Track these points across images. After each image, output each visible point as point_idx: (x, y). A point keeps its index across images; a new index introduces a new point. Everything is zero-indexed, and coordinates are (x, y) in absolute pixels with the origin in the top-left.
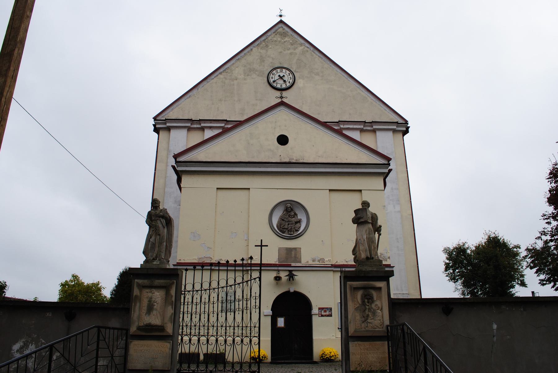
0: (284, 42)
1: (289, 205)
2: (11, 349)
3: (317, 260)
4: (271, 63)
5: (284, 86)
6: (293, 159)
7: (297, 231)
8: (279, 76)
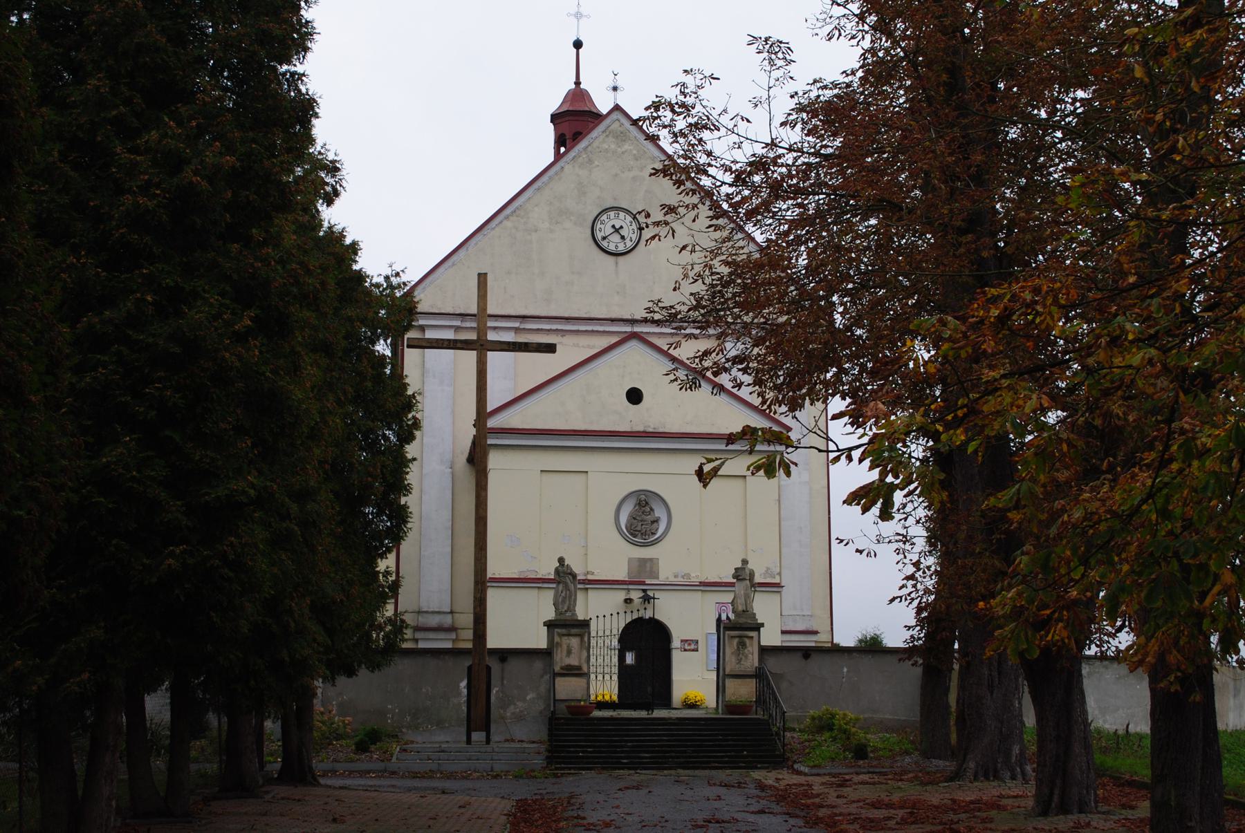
0: (623, 153)
1: (643, 497)
2: (459, 686)
3: (680, 576)
4: (599, 197)
5: (621, 248)
6: (649, 427)
7: (654, 534)
8: (613, 226)
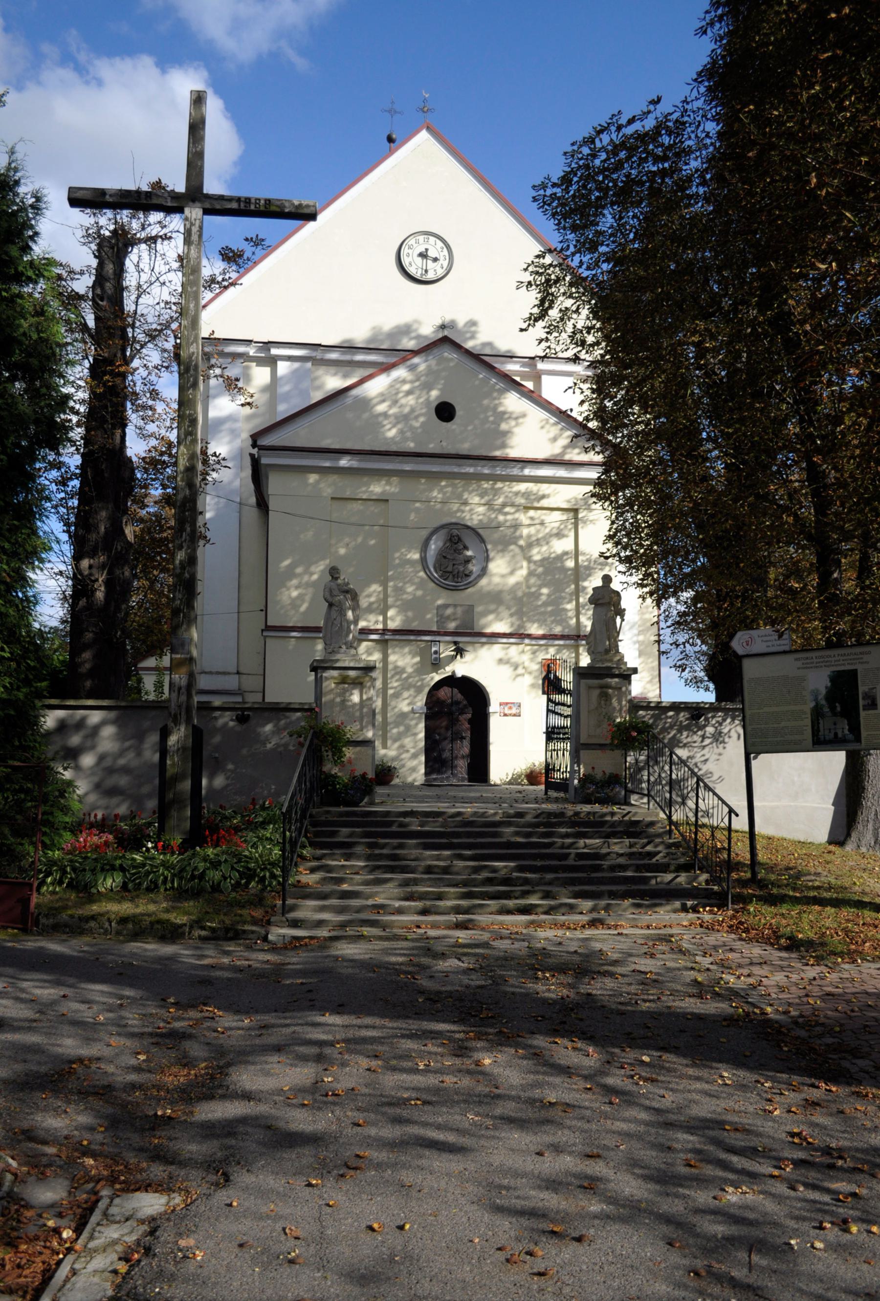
1: (455, 532)
